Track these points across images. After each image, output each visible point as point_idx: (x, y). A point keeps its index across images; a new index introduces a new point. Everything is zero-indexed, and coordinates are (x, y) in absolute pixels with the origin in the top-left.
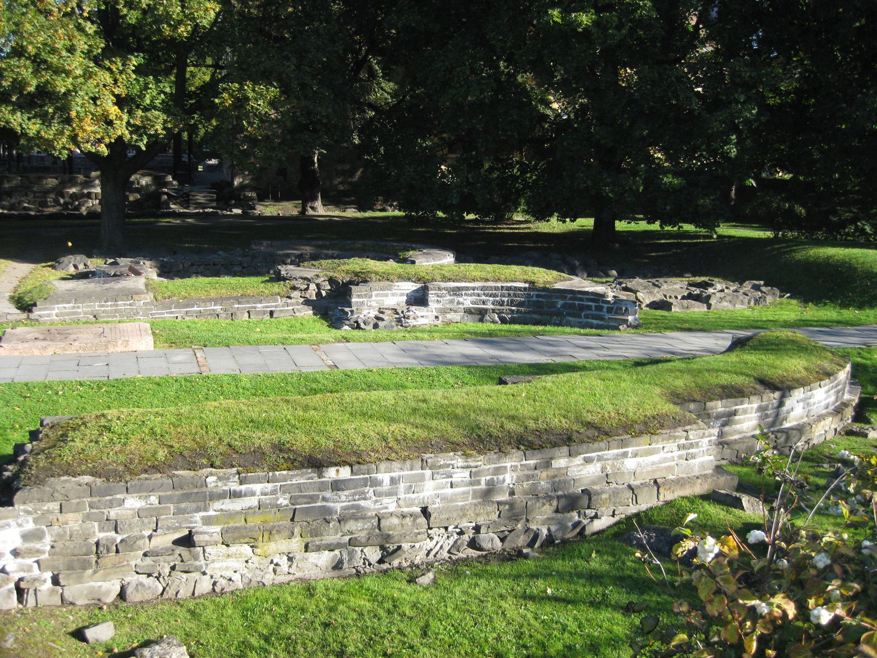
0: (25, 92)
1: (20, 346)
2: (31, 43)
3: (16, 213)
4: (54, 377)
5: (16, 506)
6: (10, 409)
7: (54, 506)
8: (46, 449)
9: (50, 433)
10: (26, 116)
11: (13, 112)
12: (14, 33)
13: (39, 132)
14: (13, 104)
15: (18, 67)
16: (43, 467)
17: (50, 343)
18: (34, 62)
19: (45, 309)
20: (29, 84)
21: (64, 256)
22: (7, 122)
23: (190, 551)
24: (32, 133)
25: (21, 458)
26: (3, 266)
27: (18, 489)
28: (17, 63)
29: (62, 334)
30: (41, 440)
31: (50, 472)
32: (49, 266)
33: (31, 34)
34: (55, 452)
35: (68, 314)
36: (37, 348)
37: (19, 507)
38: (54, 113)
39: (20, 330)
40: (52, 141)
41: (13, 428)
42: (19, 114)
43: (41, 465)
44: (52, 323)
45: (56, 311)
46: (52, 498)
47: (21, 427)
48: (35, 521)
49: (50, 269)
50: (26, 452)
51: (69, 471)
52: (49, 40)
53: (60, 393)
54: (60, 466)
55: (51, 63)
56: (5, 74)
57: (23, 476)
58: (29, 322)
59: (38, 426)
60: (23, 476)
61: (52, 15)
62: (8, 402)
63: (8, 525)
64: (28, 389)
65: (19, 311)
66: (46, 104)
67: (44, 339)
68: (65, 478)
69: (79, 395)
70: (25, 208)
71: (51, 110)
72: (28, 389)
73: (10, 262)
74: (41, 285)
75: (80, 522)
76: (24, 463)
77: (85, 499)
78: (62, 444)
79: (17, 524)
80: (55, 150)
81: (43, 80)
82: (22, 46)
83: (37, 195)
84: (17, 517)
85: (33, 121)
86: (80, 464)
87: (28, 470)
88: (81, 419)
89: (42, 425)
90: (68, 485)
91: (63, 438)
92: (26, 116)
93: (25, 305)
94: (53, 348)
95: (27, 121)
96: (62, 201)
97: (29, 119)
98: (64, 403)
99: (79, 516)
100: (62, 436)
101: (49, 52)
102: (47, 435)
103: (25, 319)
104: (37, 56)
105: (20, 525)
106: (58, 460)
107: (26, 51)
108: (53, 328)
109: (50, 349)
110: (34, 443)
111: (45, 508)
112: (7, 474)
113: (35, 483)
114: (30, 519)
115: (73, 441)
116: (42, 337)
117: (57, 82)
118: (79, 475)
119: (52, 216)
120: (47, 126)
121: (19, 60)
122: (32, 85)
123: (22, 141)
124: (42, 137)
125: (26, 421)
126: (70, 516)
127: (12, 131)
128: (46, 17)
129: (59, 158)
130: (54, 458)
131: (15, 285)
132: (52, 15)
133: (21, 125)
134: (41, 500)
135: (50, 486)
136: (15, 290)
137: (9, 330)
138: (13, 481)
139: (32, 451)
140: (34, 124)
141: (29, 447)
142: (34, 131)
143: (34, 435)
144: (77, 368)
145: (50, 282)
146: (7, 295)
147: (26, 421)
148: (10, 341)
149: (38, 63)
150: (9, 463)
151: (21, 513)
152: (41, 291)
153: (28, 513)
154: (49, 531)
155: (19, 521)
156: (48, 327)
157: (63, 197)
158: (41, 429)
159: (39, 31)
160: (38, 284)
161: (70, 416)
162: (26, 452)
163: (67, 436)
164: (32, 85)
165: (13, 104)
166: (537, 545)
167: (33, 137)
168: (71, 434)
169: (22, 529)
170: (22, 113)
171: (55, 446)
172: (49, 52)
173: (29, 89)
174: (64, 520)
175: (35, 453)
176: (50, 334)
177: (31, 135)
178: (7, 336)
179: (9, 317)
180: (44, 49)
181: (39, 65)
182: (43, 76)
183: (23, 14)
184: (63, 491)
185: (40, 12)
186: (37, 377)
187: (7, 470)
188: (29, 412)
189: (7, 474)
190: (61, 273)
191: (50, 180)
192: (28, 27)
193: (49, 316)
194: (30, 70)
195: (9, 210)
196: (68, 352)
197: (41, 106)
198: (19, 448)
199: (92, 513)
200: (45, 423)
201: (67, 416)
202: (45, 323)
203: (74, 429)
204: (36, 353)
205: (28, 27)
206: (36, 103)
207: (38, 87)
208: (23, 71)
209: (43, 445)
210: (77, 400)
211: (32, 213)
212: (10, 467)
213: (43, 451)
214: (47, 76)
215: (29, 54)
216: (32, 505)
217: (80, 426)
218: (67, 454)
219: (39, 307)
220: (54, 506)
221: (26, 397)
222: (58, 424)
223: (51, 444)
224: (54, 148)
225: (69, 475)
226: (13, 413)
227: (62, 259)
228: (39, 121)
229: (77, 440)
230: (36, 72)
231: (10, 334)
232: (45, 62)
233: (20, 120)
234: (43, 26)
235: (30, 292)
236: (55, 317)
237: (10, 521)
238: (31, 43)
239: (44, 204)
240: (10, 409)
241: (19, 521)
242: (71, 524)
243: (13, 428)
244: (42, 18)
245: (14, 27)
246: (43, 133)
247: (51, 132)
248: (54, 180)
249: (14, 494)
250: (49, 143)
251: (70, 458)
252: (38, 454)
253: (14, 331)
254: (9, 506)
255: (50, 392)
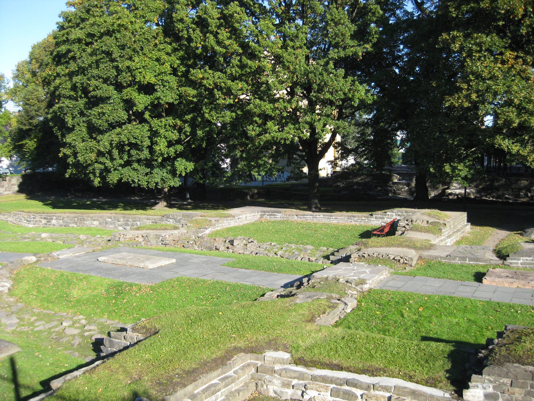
0: (511, 127)
1: (497, 280)
2: (517, 97)
3: (501, 200)
4: (516, 301)
5: (484, 376)
6: (487, 317)
7: (507, 381)
8: (506, 344)
9: (510, 335)
10: (511, 142)
11: (504, 139)
12: (506, 92)
13: (518, 151)
14: (504, 134)
15: (508, 112)
16: (504, 355)
17: (516, 280)
18: (517, 108)
19: (514, 259)
20: (514, 122)
21: (529, 228)
22: (500, 145)
23: (33, 389)
24: (514, 151)
25: (491, 347)
26: (490, 231)
27: (486, 366)
28: (507, 110)
29: (523, 275)
30: (504, 338)
31: (508, 359)
32: (519, 234)
33: (516, 92)
34: (512, 347)
35: (528, 264)
36: (507, 282)
37: (485, 377)
38: (529, 140)
39: (498, 270)
40: (526, 157)
41: (487, 328)
42: (507, 140)
43: (502, 353)
44: (518, 268)
45: (521, 261)
46: (507, 376)
47: (492, 329)
48: (494, 388)
49: (519, 235)
50: (494, 344)
51: (520, 361)
52: (528, 95)
53: (519, 312)
54: (514, 357)
55: (529, 109)
56: (500, 116)
57: (490, 358)
58: (503, 266)
59: (503, 329)
60: (490, 358)
61: (530, 80)
62: (486, 312)
63: (477, 387)
64: (499, 306)
65: (498, 259)
66: (523, 134)
67: (512, 278)
68: (517, 365)
69: (531, 315)
70: (506, 198)
71: (526, 138)
72: (499, 306)
73: (495, 229)
74: (513, 245)
75: (523, 395)
76: (492, 350)
77: (528, 381)
78: (517, 343)
79: (483, 387)
80: (528, 162)
81: (523, 119)
82: (511, 100)
83: (514, 190)
84: (483, 382)
85: (515, 144)
86: (528, 358)
87: (493, 355)
88: (532, 329)
89: (506, 329)
90: (518, 369)
91: (519, 339)
92: (511, 142)
93: (502, 255)
94: (517, 284)
95: (511, 145)
96: (529, 195)
97: (513, 143)
98: (521, 319)
99: (523, 391)
100: (518, 338)
101: (527, 102)
102: (508, 336)
103: (501, 264)
104: (519, 105)
105: (484, 388)
106: (513, 353)
107: (513, 102)
108: (518, 271)
109: (515, 284)
110: (500, 339)
111: (501, 381)
112: (480, 355)
113: (497, 364)
114: (491, 385)
115: (525, 342)
116: (510, 276)
117: (531, 121)
118: (526, 364)
119: (523, 203)
120: (524, 148)
121: (509, 108)
122: (515, 123)
123: (508, 157)
124: (520, 154)
125: (495, 325)
126: (517, 390)
127: (502, 151)
128: (526, 81)
129: (530, 167)
130: (511, 351)
131: (496, 243)
132: (530, 80)
133: (507, 147)
134: (499, 376)
135: (506, 368)
136: (497, 246)
137: (491, 269)
138: (484, 360)
139: (498, 344)
140: (516, 146)
141: (496, 341)
142: (515, 150)
143: (500, 335)
144: (531, 298)
145: (519, 243)
146: (491, 248)
147: (495, 325)
148: (491, 276)
149: (520, 109)
150: (483, 349)
151: (486, 381)
152: (512, 248)
153: (490, 382)
154: (502, 396)
155: (484, 385)
156: (515, 270)
157: (530, 192)
158: (505, 331)
159: (521, 90)
160: (510, 244)
161: (524, 327)
162: (494, 344)
163: (521, 339)
164: (515, 123)
165: (504, 134)
166: (372, 386)
167: (514, 154)
168: (524, 337)
169: (485, 391)
170: (509, 140)
171: (512, 343)
172: (527, 102)
173: (514, 125)
174: (512, 391)
175: (500, 346)
176: (516, 275)
177: (514, 153)
178: (489, 272)
179: (491, 262)
180: (524, 100)
181: (520, 111)
182: (523, 117)
183: (513, 80)
184: (514, 373)
185: (523, 78)
186: (505, 300)
187: (481, 353)
188: (498, 320)
189: (480, 355)
190: (525, 239)
191: (523, 182)
192: (515, 88)
193: (516, 263)
194: (515, 114)
195: (497, 198)
196: (526, 287)
197: (521, 135)
198: (490, 341)
199: (531, 391)
200: (508, 328)
201: (522, 326)
202: (513, 268)
203: (526, 335)
204: (506, 285)
205: (515, 88)
206: (517, 134)
207: (519, 124)
208: (511, 114)
209: (505, 341)
210: (529, 318)
211: (511, 201)
212: (483, 351)
213: (505, 345)
214: (525, 117)
215: (515, 104)
216: (493, 377)
217: (530, 334)
218: (519, 350)
219: (510, 257)
220: (507, 381)
221: (497, 311)
222: (516, 330)
223: (510, 341)
224: (527, 161)
225: (520, 363)
226: (488, 320)
227: (527, 230)
228: (519, 145)
229: (528, 342)
230: (519, 115)
231: (491, 271)
232: (525, 108)
233: (507, 144)
234: (524, 87)
235: (506, 248)
236: (520, 265)
237: (478, 384)
238: (517, 97)
239: (518, 196)
240: (487, 317)
241: (484, 385)
242: (517, 395)
243: (487, 328)
244: (524, 82)
245: (506, 89)
246: (521, 152)
247: (526, 151)
248: (525, 181)
249: (484, 368)
250: (525, 158)
251: (522, 353)
252: (501, 346)
253: (494, 270)
254: (479, 375)
255: (512, 310)
